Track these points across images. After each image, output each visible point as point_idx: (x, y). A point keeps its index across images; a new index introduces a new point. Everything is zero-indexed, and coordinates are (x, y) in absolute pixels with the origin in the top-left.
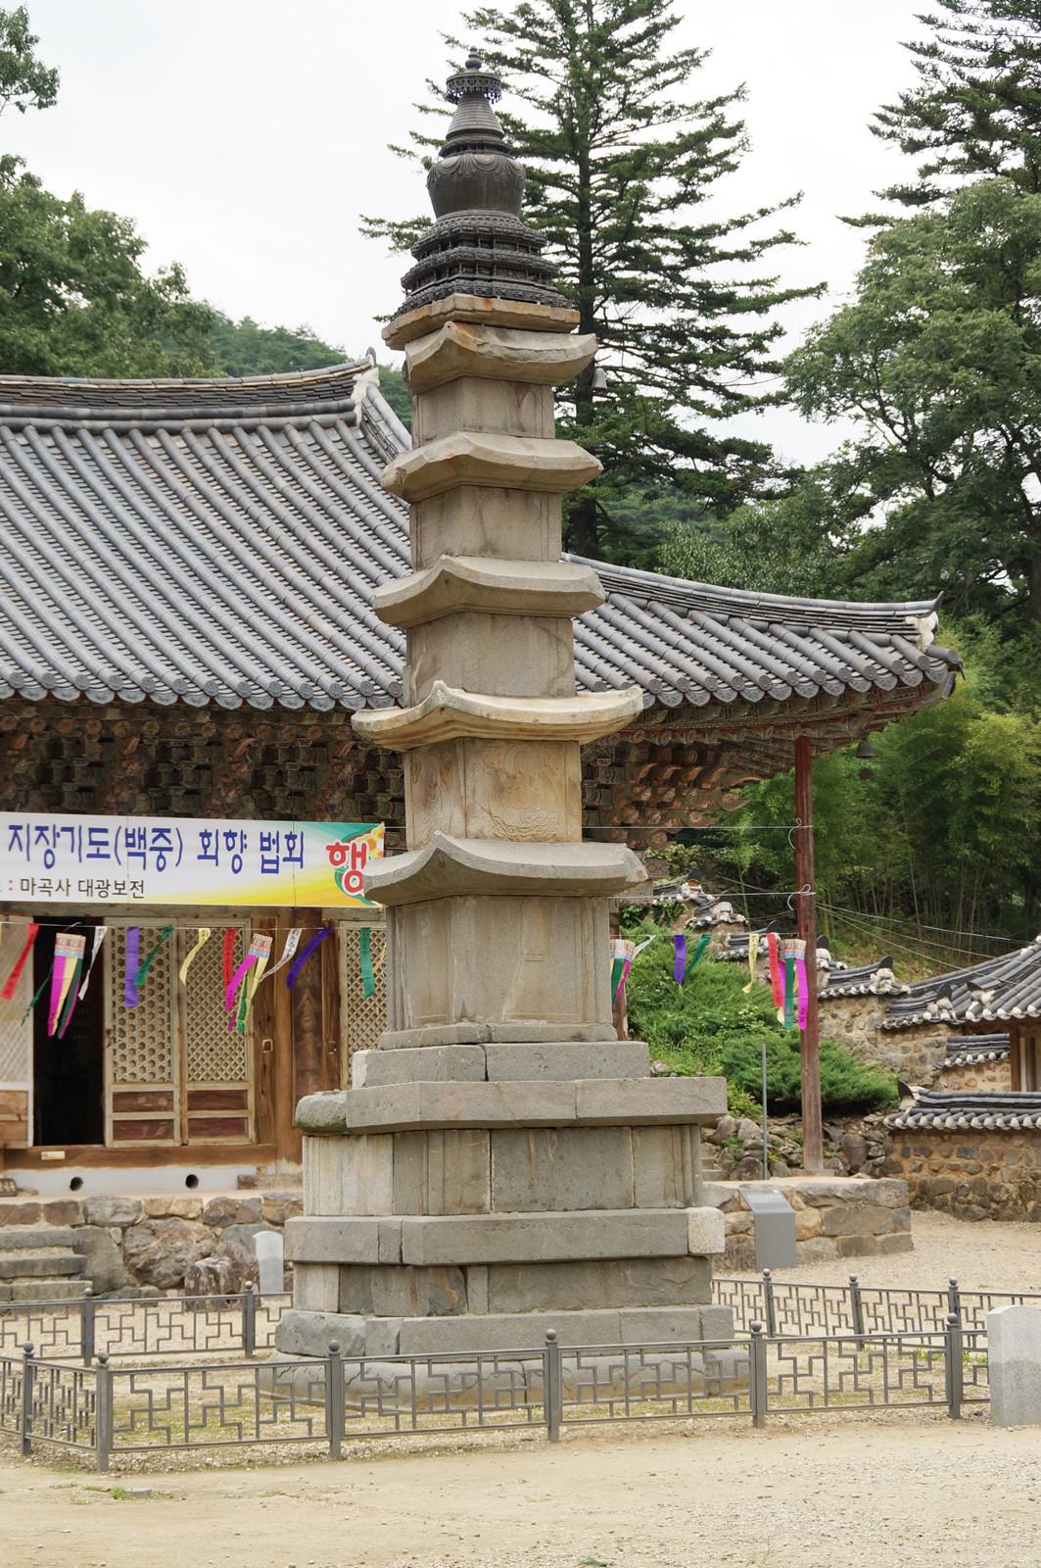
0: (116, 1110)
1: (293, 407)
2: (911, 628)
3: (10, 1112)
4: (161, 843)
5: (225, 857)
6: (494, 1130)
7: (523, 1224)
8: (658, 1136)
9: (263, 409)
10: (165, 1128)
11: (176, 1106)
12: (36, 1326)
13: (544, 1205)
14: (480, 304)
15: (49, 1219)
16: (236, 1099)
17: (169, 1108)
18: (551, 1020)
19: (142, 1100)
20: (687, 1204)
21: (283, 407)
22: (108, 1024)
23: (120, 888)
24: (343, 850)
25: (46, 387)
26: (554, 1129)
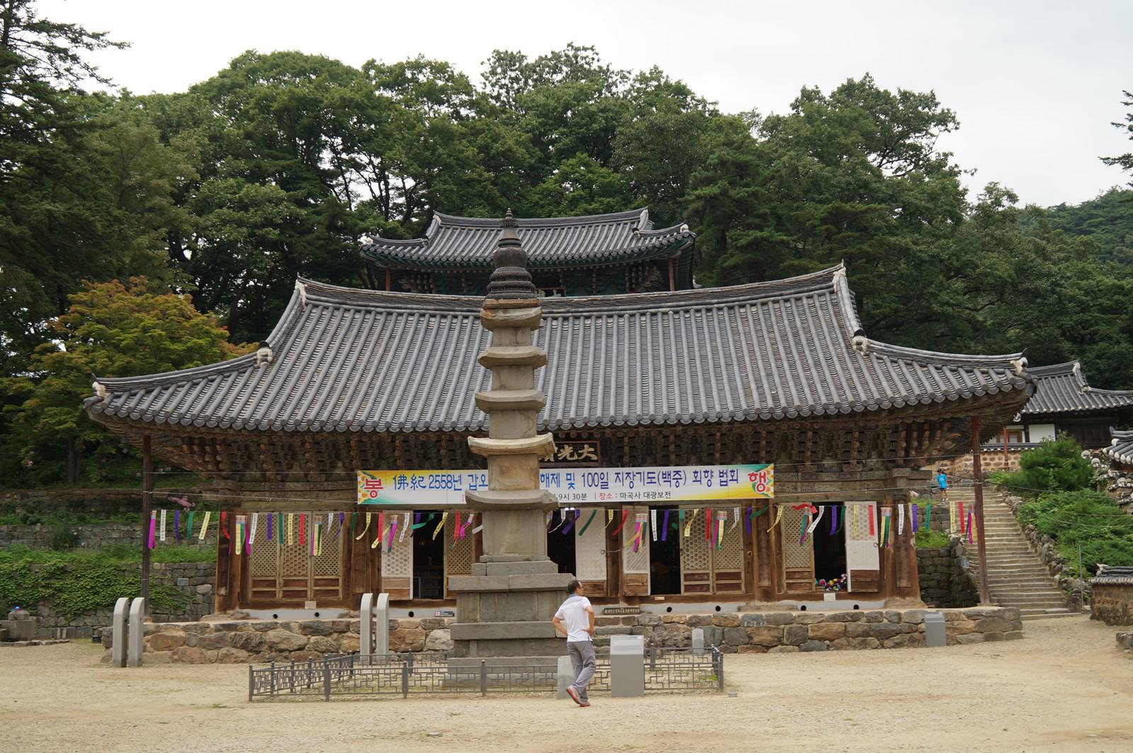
0: (685, 580)
1: (806, 289)
2: (1012, 365)
3: (638, 582)
4: (677, 476)
5: (704, 481)
6: (482, 593)
7: (489, 626)
8: (549, 594)
9: (792, 291)
10: (707, 588)
11: (711, 579)
14: (494, 302)
15: (624, 623)
16: (737, 576)
17: (708, 580)
18: (520, 554)
19: (696, 577)
21: (802, 289)
22: (681, 547)
23: (661, 495)
24: (755, 475)
25: (699, 293)
26: (505, 593)
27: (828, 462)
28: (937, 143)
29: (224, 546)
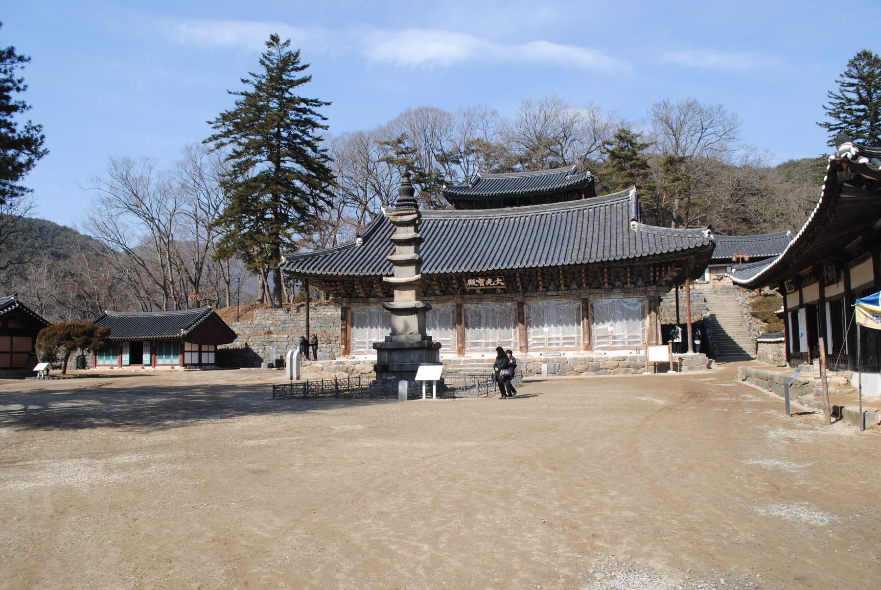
16: (573, 338)
27: (617, 284)
28: (828, 129)
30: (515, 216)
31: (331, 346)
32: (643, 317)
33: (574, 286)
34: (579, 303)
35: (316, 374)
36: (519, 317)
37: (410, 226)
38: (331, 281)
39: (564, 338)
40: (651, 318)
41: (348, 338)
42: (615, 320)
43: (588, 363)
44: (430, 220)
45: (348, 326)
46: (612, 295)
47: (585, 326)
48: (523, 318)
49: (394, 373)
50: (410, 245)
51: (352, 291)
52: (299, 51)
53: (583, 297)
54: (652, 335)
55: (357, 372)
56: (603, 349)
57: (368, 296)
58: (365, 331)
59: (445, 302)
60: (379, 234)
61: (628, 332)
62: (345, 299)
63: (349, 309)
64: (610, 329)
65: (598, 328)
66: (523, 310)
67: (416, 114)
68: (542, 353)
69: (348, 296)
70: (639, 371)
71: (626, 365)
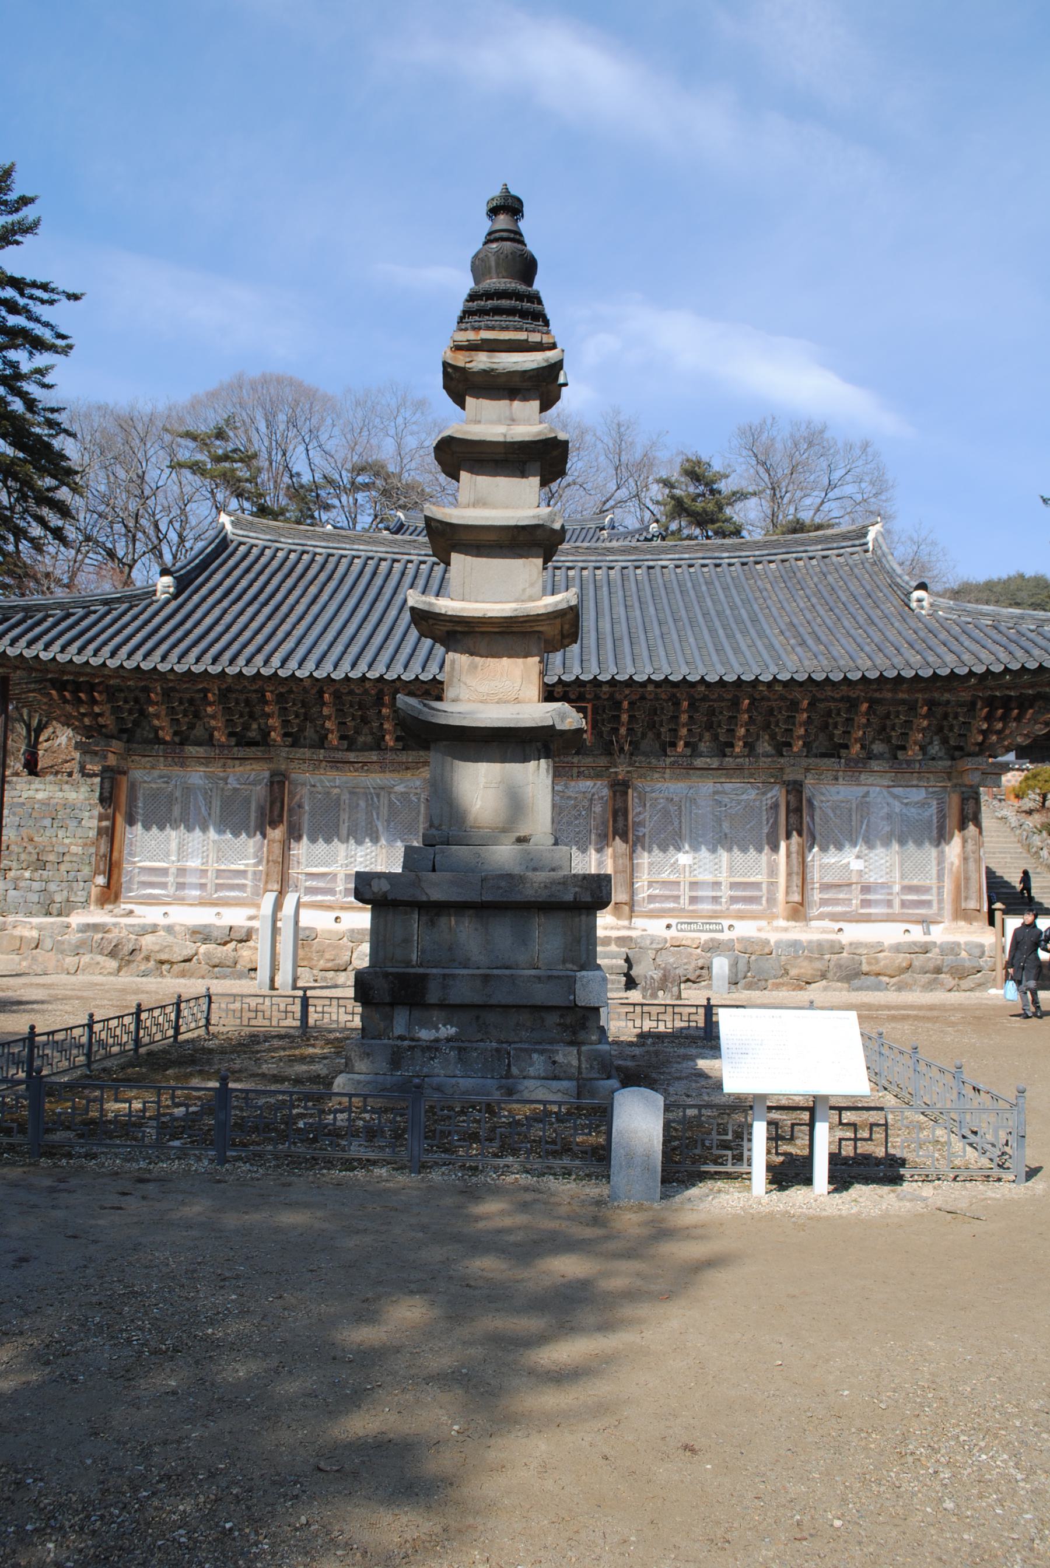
1: (835, 545)
12: (334, 1018)
13: (460, 963)
16: (757, 885)
20: (583, 968)
29: (105, 823)
30: (581, 564)
31: (45, 877)
32: (941, 837)
33: (764, 746)
34: (778, 794)
35: (17, 958)
36: (615, 821)
37: (525, 399)
38: (77, 687)
39: (733, 886)
40: (964, 841)
41: (115, 854)
42: (870, 845)
43: (827, 957)
44: (354, 557)
45: (120, 820)
46: (863, 777)
47: (794, 856)
48: (626, 826)
49: (451, 1009)
50: (523, 475)
51: (136, 723)
52: (13, 165)
53: (789, 777)
54: (967, 888)
55: (147, 959)
56: (834, 917)
57: (183, 739)
58: (168, 840)
59: (407, 769)
60: (218, 576)
61: (902, 877)
62: (117, 745)
63: (125, 773)
64: (856, 865)
65: (825, 861)
66: (626, 801)
67: (254, 389)
68: (673, 922)
69: (125, 736)
70: (966, 983)
71: (931, 965)
